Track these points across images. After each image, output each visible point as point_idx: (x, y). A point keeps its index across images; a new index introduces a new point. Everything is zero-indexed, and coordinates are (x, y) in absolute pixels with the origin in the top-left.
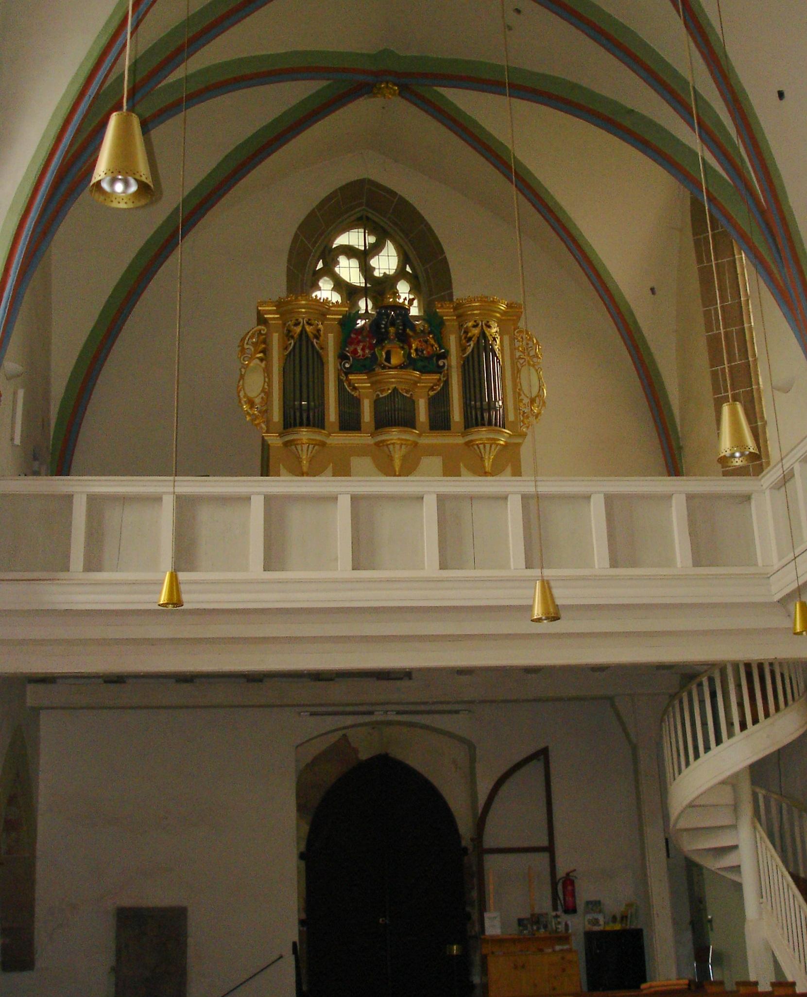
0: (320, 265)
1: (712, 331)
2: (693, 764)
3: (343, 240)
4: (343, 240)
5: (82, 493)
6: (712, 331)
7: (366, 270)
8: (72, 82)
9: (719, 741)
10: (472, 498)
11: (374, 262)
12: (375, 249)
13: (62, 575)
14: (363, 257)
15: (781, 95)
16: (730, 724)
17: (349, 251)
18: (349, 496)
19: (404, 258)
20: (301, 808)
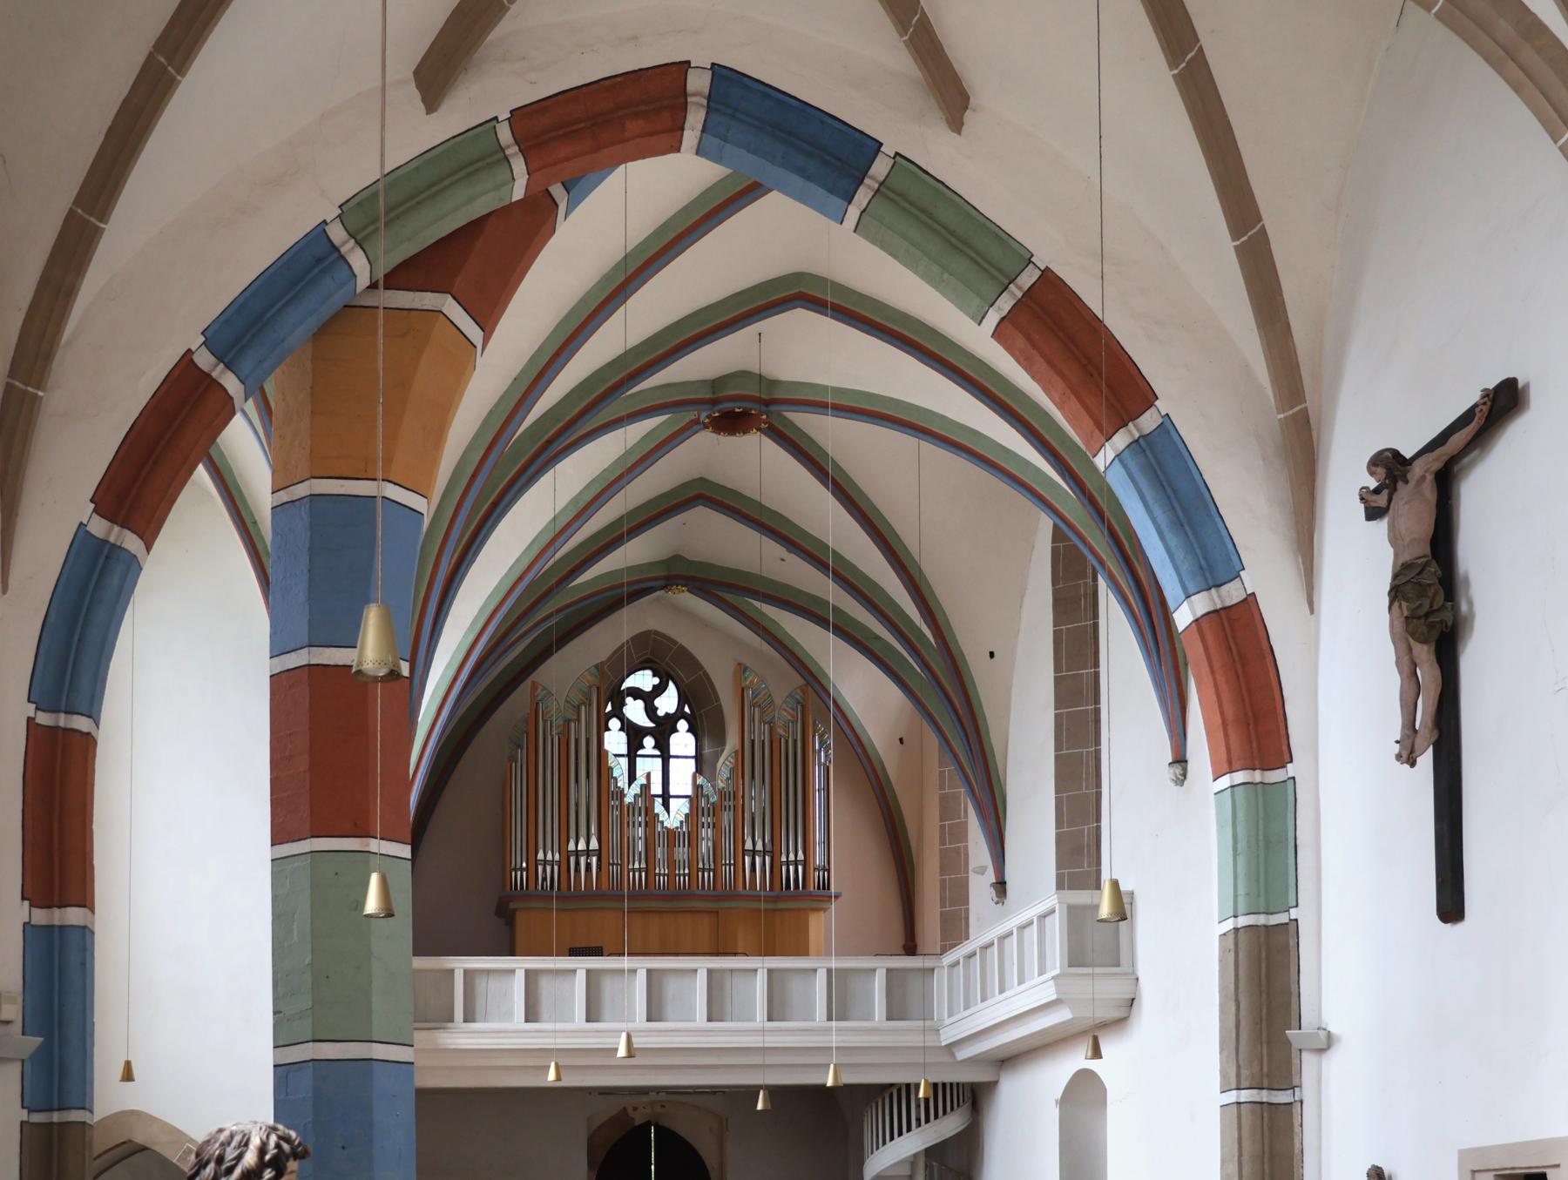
0: (609, 708)
1: (945, 790)
2: (881, 1149)
3: (631, 682)
4: (631, 682)
5: (460, 968)
6: (945, 790)
7: (651, 711)
8: (447, 667)
9: (909, 1130)
10: (732, 971)
11: (657, 702)
12: (659, 690)
13: (450, 1025)
14: (648, 698)
15: (992, 655)
16: (918, 1120)
17: (636, 693)
18: (645, 970)
19: (682, 700)
20: (590, 1164)
